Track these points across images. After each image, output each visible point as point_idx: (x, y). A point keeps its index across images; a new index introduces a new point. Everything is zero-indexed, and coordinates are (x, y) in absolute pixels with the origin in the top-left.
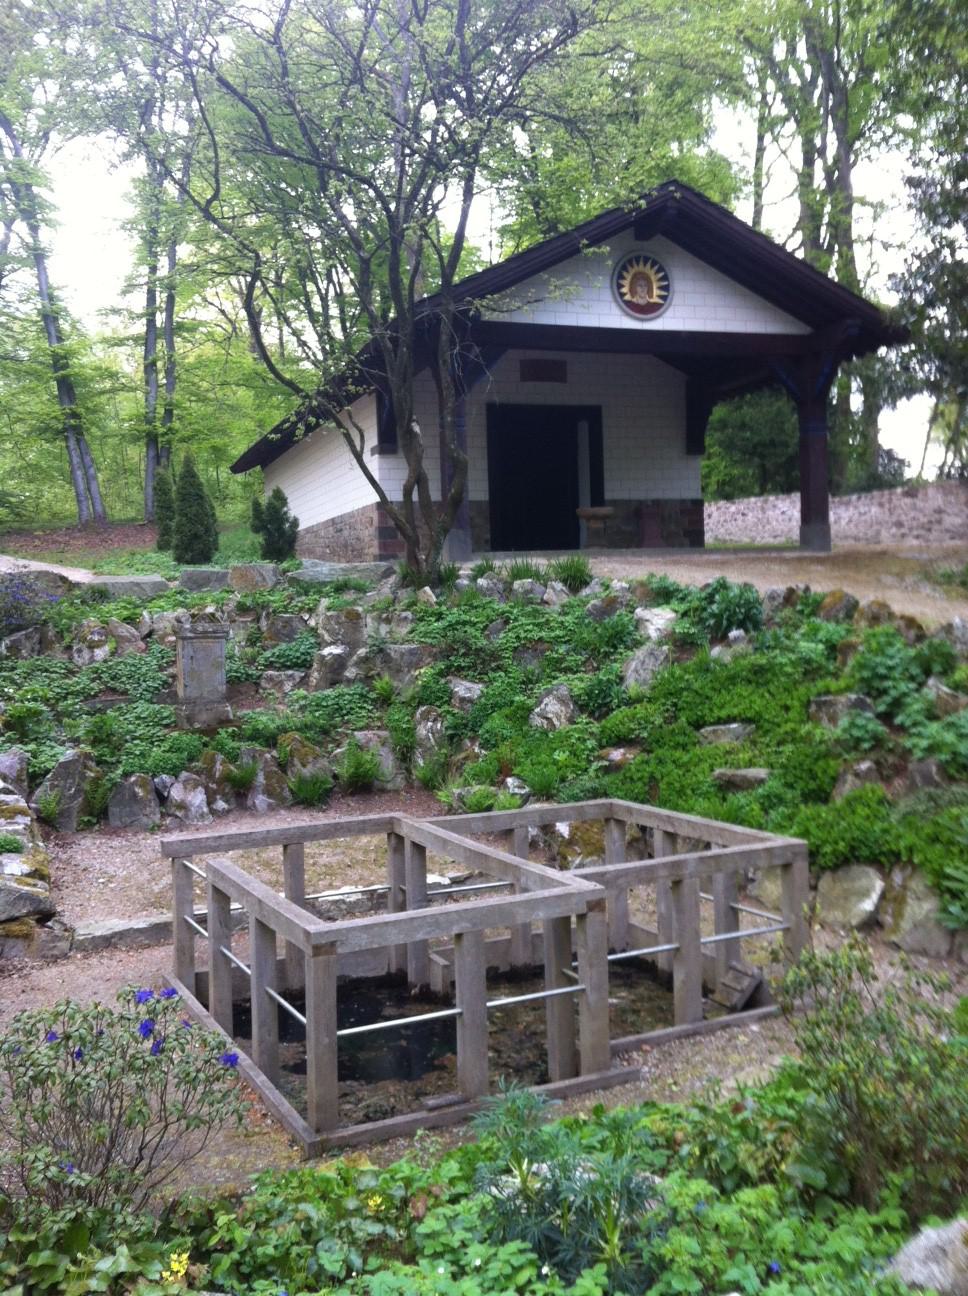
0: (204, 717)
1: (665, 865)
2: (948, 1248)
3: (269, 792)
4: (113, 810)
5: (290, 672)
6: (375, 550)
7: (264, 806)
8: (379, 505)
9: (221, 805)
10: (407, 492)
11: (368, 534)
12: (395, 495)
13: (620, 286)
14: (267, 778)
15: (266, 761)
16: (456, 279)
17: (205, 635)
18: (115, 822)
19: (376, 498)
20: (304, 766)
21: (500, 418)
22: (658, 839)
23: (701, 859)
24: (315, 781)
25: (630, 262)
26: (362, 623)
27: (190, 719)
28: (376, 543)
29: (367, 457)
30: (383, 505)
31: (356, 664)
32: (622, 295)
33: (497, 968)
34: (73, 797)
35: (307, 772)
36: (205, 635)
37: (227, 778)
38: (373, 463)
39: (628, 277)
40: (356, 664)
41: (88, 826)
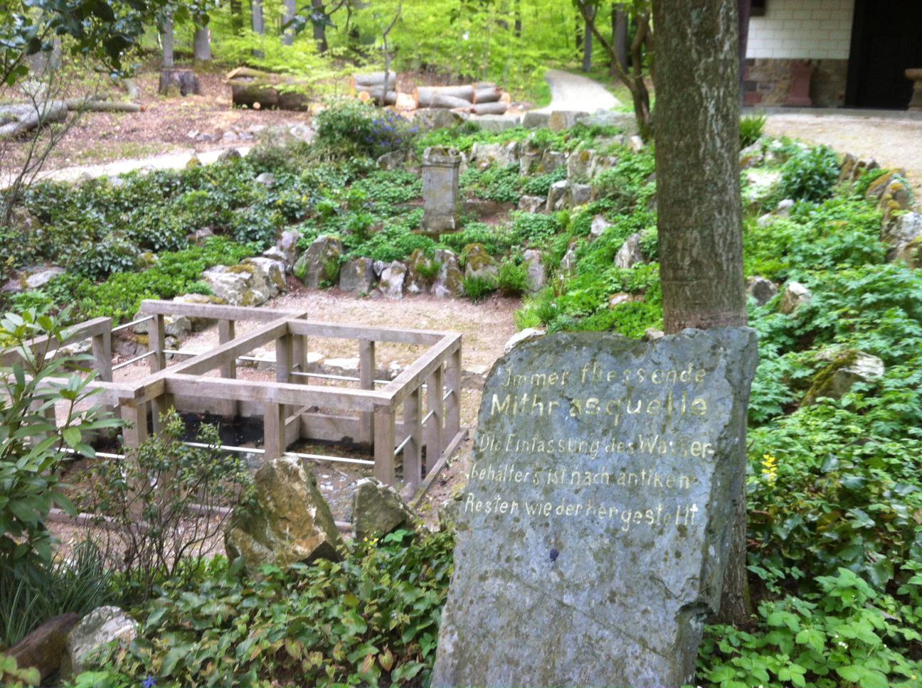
0: (434, 224)
1: (246, 387)
3: (449, 285)
4: (343, 279)
5: (535, 198)
7: (442, 294)
9: (414, 288)
14: (449, 274)
15: (450, 262)
17: (438, 164)
18: (343, 287)
20: (475, 269)
23: (280, 390)
24: (481, 283)
26: (589, 163)
27: (425, 225)
33: (351, 439)
34: (317, 267)
35: (475, 274)
36: (438, 164)
37: (420, 271)
41: (324, 287)
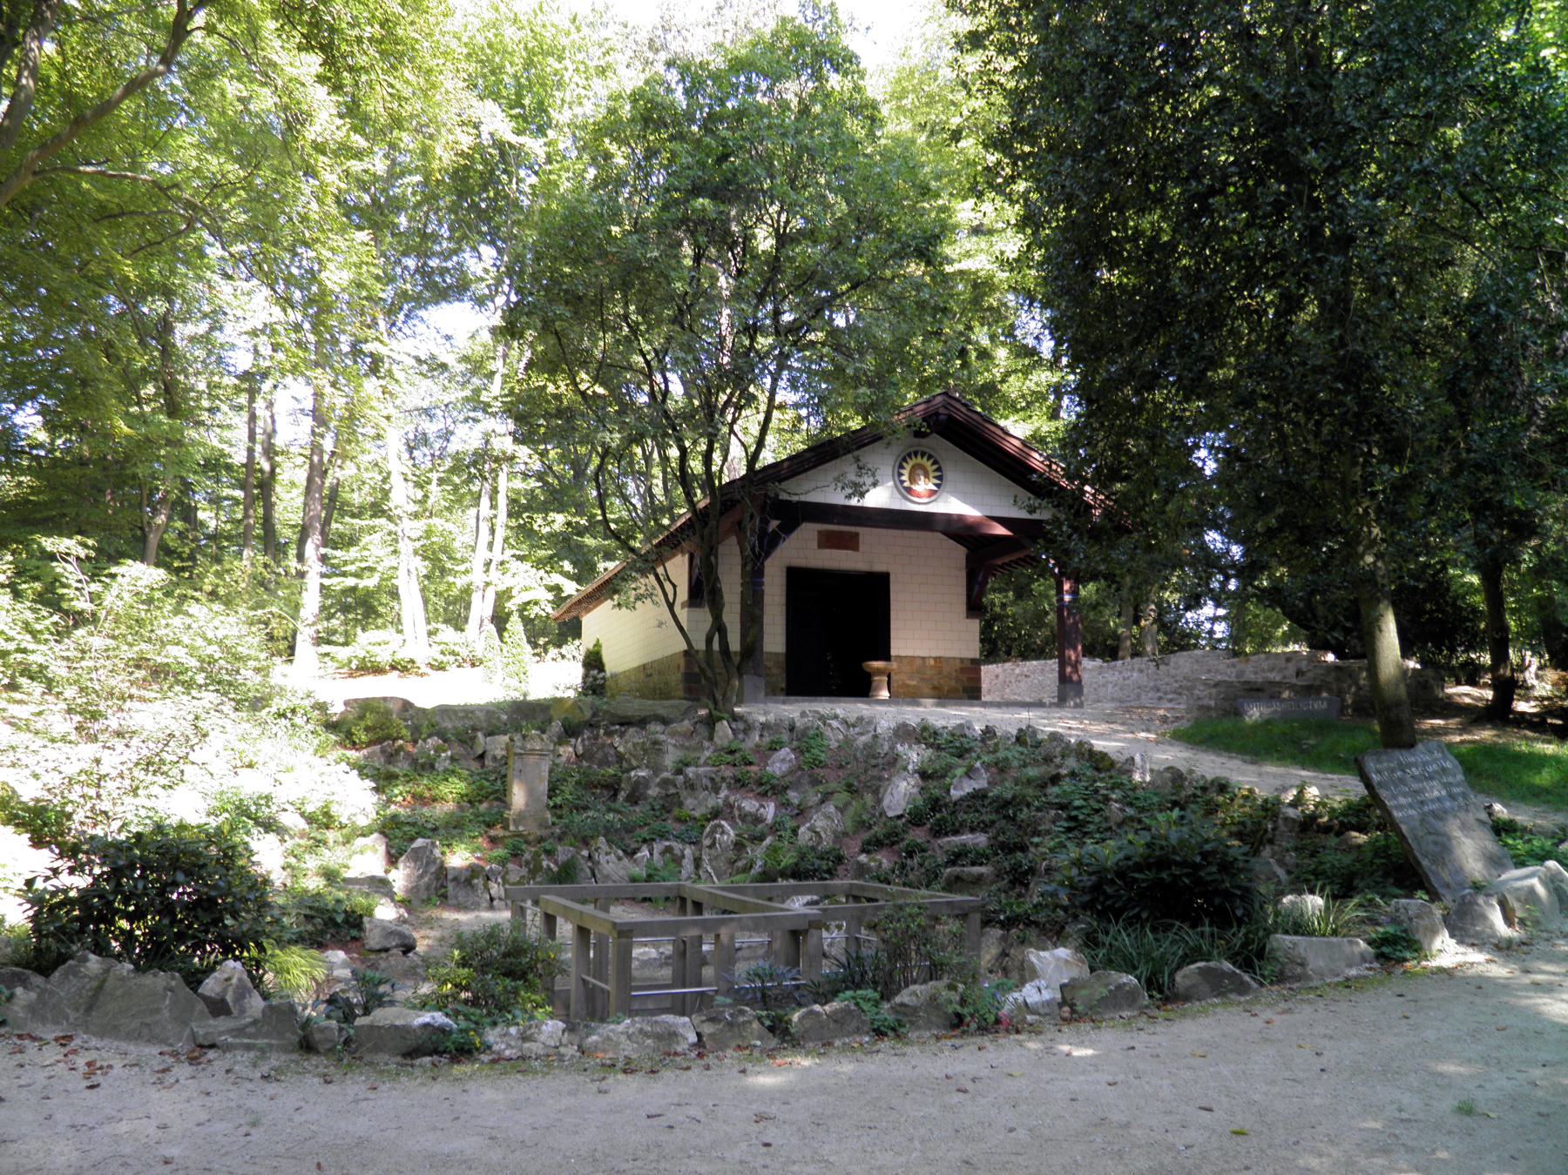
2: (50, 1123)
6: (681, 693)
8: (686, 653)
10: (709, 641)
11: (676, 678)
12: (700, 645)
13: (900, 475)
16: (758, 466)
19: (684, 646)
21: (796, 577)
22: (689, 906)
25: (909, 455)
28: (681, 686)
29: (677, 608)
30: (689, 654)
31: (659, 785)
32: (902, 482)
38: (683, 614)
39: (908, 467)
40: (659, 785)
